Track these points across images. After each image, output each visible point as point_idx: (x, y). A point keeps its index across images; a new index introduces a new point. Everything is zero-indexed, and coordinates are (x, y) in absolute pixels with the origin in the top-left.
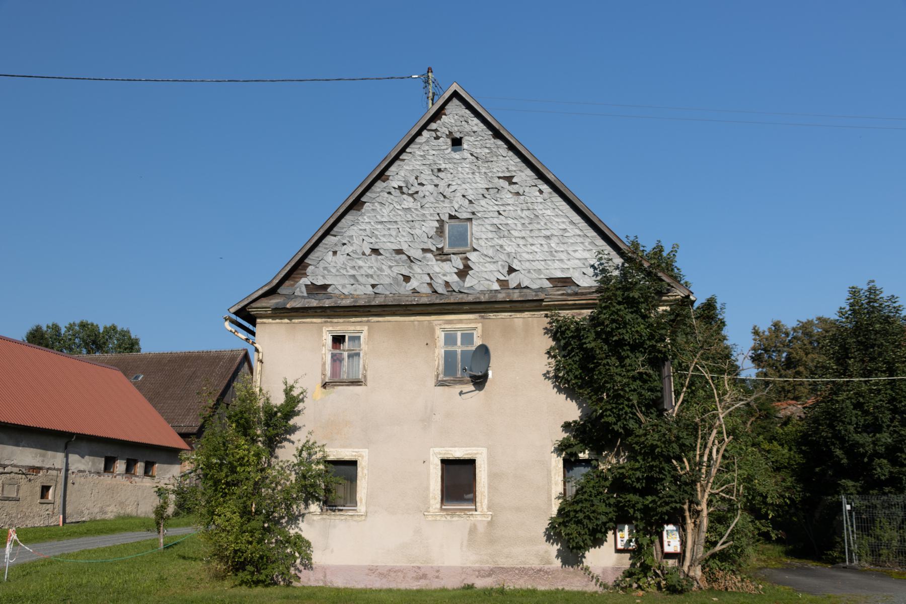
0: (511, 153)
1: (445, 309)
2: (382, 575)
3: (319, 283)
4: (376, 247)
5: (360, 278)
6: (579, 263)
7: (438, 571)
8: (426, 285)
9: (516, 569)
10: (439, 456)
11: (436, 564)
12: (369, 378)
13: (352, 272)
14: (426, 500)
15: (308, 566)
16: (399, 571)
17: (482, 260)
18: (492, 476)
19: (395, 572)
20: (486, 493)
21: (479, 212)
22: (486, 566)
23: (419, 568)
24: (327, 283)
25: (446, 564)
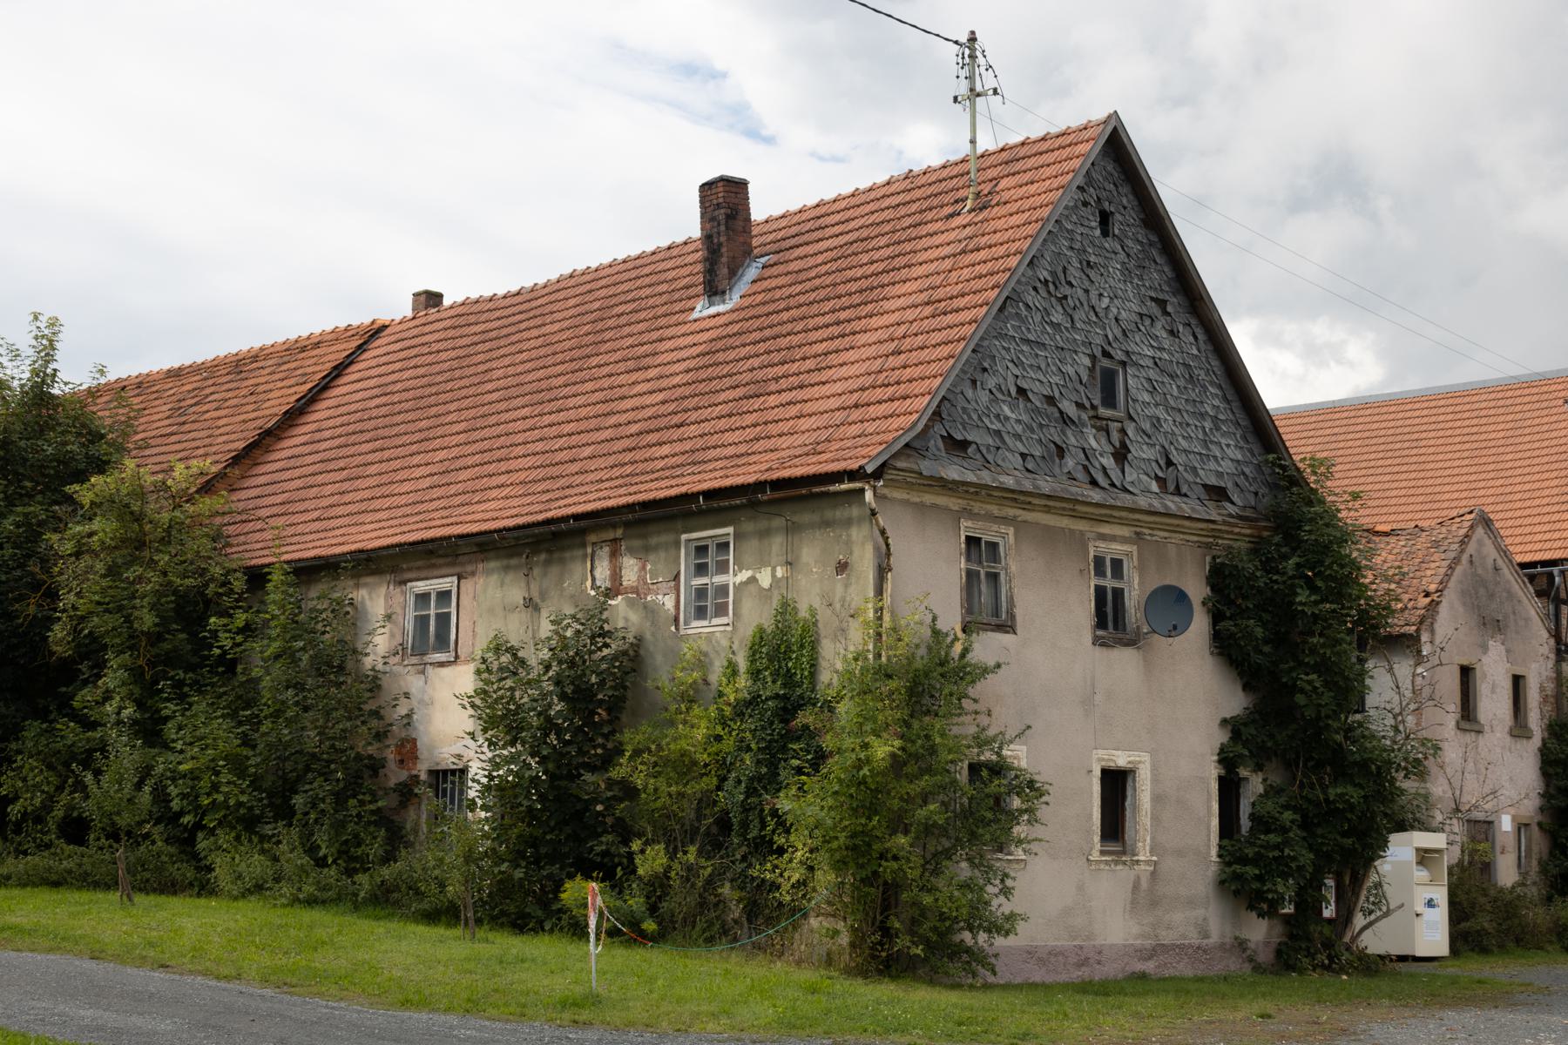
0: (1125, 189)
1: (1183, 527)
2: (1042, 962)
3: (959, 437)
4: (1025, 386)
5: (1006, 438)
6: (1098, 340)
7: (1100, 953)
8: (1080, 467)
9: (1177, 946)
10: (1103, 763)
11: (1099, 942)
12: (1019, 619)
13: (996, 426)
14: (1089, 832)
15: (1006, 892)
16: (1061, 953)
17: (1140, 439)
18: (1157, 799)
19: (1056, 955)
20: (1148, 827)
21: (1134, 353)
22: (1149, 943)
23: (1081, 947)
24: (969, 438)
25: (1109, 942)
